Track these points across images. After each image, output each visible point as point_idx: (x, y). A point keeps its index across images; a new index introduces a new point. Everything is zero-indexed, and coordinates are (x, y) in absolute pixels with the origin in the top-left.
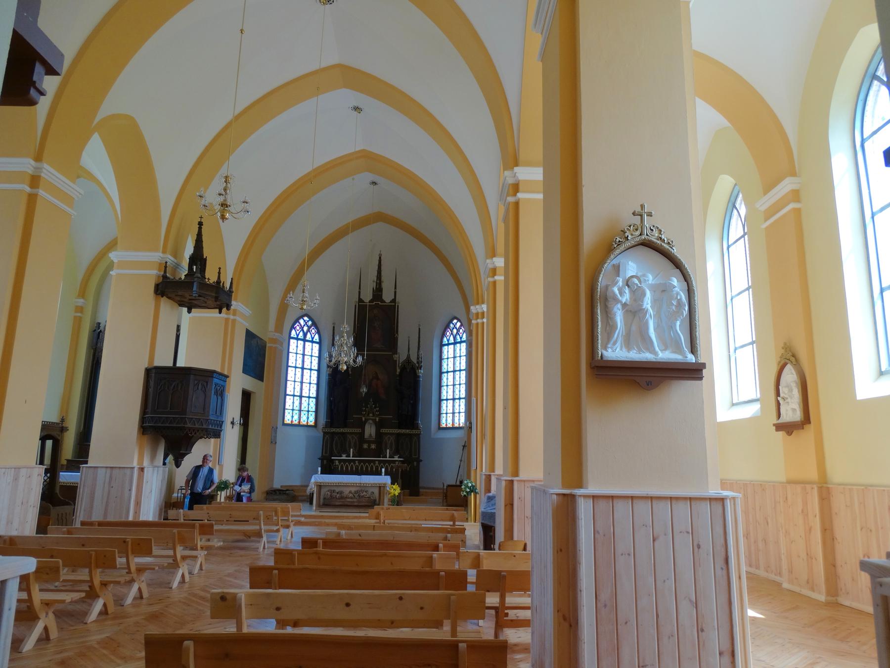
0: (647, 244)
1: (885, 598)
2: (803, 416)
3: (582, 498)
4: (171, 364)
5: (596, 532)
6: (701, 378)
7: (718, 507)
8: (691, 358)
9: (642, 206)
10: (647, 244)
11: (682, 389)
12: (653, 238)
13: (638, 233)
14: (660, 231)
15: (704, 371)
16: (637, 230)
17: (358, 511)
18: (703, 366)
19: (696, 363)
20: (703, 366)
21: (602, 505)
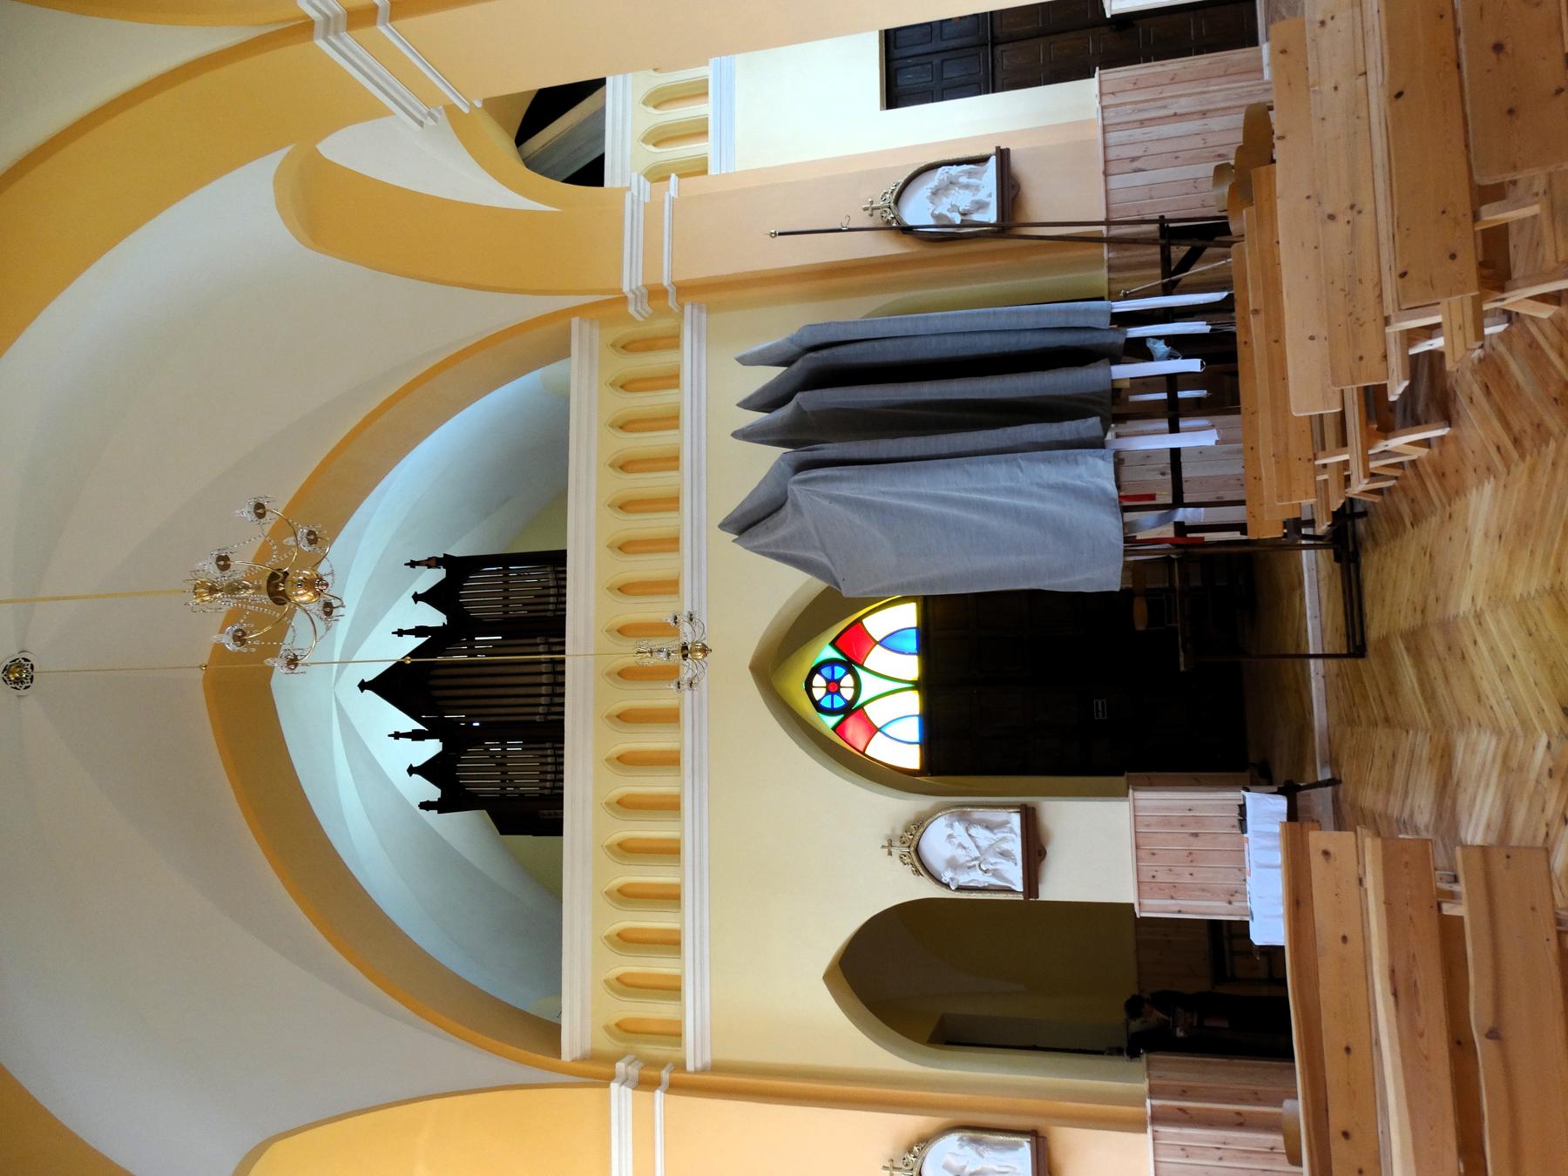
0: (897, 201)
1: (985, 1174)
2: (1101, 362)
3: (1105, 246)
4: (918, 746)
5: (1146, 154)
6: (1008, 150)
7: (1112, 281)
8: (993, 160)
9: (866, 209)
10: (897, 201)
11: (1018, 164)
12: (891, 198)
13: (888, 210)
14: (886, 193)
15: (1002, 148)
16: (885, 211)
17: (916, 342)
18: (998, 148)
19: (996, 154)
20: (998, 148)
21: (1113, 168)
